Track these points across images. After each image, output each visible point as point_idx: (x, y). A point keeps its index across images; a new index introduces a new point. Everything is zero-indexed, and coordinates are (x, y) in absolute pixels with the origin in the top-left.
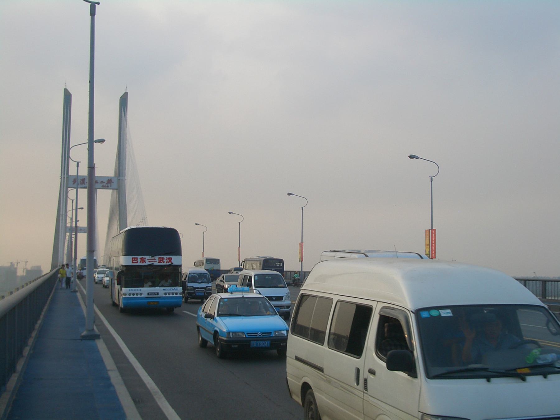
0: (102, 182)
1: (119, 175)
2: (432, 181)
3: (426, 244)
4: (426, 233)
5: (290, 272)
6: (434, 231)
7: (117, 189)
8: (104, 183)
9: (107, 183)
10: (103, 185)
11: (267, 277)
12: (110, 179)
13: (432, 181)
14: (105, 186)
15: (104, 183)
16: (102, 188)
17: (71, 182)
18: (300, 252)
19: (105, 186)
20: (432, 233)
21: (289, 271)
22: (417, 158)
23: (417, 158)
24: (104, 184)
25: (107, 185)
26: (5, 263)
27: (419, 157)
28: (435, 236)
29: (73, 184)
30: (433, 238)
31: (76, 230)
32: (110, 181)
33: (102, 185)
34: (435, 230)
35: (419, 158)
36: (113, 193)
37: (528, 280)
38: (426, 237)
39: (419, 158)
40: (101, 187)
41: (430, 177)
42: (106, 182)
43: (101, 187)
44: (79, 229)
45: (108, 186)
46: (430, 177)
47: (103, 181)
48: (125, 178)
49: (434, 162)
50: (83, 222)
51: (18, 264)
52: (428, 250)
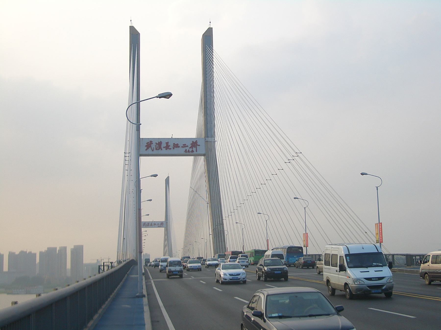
0: (185, 146)
1: (207, 136)
2: (377, 190)
3: (376, 233)
4: (375, 226)
5: (316, 255)
6: (307, 234)
7: (204, 155)
8: (187, 146)
9: (192, 147)
10: (186, 150)
11: (348, 261)
12: (194, 141)
13: (377, 190)
14: (189, 151)
15: (187, 146)
16: (185, 153)
17: (143, 148)
18: (305, 240)
19: (189, 151)
20: (379, 226)
21: (314, 255)
22: (366, 174)
23: (366, 174)
24: (187, 149)
25: (191, 150)
26: (2, 253)
27: (368, 173)
28: (382, 227)
29: (146, 150)
30: (307, 237)
31: (102, 266)
32: (194, 143)
33: (185, 149)
34: (381, 223)
35: (368, 174)
36: (195, 162)
37: (395, 255)
38: (376, 229)
39: (368, 174)
40: (183, 153)
41: (376, 187)
42: (190, 146)
43: (183, 153)
44: (142, 224)
45: (193, 151)
46: (376, 187)
47: (185, 145)
48: (214, 139)
49: (379, 177)
50: (103, 265)
51: (307, 247)
52: (377, 237)
